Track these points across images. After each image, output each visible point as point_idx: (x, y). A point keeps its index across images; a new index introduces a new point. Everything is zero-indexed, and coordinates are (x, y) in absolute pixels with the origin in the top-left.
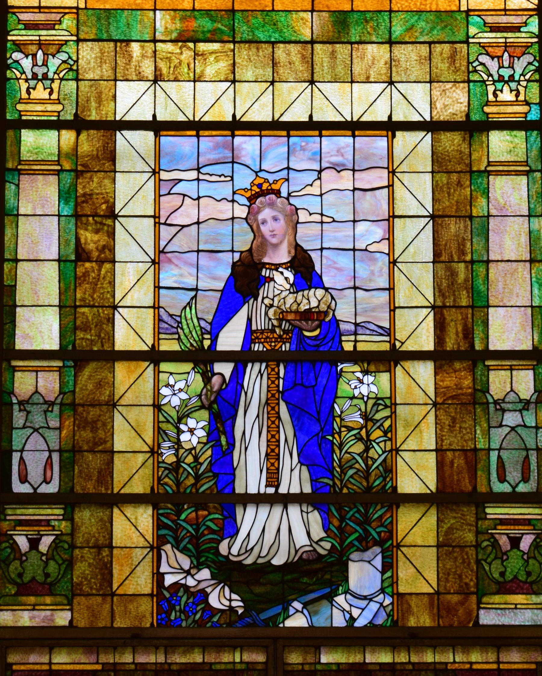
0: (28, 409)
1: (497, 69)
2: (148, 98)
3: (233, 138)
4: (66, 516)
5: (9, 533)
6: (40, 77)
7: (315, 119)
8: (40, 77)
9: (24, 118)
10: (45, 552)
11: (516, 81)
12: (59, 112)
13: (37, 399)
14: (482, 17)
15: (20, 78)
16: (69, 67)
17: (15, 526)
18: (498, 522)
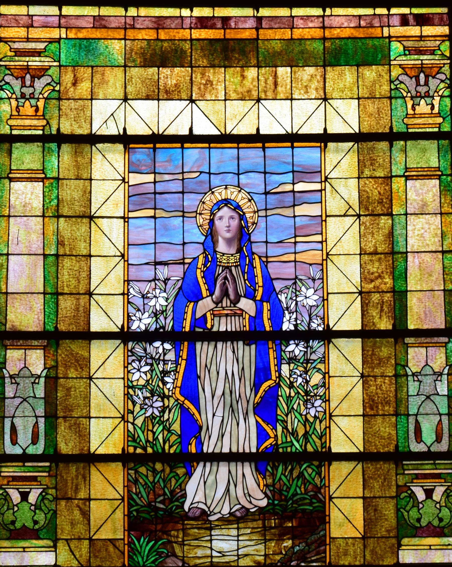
0: (420, 380)
1: (415, 87)
2: (253, 114)
3: (293, 149)
4: (51, 473)
5: (408, 484)
6: (28, 97)
7: (262, 132)
8: (28, 97)
9: (410, 131)
10: (34, 503)
11: (36, 98)
12: (440, 124)
13: (428, 370)
14: (402, 42)
15: (11, 98)
16: (52, 88)
17: (413, 479)
18: (414, 476)
